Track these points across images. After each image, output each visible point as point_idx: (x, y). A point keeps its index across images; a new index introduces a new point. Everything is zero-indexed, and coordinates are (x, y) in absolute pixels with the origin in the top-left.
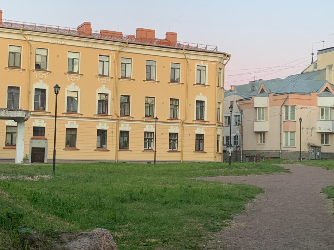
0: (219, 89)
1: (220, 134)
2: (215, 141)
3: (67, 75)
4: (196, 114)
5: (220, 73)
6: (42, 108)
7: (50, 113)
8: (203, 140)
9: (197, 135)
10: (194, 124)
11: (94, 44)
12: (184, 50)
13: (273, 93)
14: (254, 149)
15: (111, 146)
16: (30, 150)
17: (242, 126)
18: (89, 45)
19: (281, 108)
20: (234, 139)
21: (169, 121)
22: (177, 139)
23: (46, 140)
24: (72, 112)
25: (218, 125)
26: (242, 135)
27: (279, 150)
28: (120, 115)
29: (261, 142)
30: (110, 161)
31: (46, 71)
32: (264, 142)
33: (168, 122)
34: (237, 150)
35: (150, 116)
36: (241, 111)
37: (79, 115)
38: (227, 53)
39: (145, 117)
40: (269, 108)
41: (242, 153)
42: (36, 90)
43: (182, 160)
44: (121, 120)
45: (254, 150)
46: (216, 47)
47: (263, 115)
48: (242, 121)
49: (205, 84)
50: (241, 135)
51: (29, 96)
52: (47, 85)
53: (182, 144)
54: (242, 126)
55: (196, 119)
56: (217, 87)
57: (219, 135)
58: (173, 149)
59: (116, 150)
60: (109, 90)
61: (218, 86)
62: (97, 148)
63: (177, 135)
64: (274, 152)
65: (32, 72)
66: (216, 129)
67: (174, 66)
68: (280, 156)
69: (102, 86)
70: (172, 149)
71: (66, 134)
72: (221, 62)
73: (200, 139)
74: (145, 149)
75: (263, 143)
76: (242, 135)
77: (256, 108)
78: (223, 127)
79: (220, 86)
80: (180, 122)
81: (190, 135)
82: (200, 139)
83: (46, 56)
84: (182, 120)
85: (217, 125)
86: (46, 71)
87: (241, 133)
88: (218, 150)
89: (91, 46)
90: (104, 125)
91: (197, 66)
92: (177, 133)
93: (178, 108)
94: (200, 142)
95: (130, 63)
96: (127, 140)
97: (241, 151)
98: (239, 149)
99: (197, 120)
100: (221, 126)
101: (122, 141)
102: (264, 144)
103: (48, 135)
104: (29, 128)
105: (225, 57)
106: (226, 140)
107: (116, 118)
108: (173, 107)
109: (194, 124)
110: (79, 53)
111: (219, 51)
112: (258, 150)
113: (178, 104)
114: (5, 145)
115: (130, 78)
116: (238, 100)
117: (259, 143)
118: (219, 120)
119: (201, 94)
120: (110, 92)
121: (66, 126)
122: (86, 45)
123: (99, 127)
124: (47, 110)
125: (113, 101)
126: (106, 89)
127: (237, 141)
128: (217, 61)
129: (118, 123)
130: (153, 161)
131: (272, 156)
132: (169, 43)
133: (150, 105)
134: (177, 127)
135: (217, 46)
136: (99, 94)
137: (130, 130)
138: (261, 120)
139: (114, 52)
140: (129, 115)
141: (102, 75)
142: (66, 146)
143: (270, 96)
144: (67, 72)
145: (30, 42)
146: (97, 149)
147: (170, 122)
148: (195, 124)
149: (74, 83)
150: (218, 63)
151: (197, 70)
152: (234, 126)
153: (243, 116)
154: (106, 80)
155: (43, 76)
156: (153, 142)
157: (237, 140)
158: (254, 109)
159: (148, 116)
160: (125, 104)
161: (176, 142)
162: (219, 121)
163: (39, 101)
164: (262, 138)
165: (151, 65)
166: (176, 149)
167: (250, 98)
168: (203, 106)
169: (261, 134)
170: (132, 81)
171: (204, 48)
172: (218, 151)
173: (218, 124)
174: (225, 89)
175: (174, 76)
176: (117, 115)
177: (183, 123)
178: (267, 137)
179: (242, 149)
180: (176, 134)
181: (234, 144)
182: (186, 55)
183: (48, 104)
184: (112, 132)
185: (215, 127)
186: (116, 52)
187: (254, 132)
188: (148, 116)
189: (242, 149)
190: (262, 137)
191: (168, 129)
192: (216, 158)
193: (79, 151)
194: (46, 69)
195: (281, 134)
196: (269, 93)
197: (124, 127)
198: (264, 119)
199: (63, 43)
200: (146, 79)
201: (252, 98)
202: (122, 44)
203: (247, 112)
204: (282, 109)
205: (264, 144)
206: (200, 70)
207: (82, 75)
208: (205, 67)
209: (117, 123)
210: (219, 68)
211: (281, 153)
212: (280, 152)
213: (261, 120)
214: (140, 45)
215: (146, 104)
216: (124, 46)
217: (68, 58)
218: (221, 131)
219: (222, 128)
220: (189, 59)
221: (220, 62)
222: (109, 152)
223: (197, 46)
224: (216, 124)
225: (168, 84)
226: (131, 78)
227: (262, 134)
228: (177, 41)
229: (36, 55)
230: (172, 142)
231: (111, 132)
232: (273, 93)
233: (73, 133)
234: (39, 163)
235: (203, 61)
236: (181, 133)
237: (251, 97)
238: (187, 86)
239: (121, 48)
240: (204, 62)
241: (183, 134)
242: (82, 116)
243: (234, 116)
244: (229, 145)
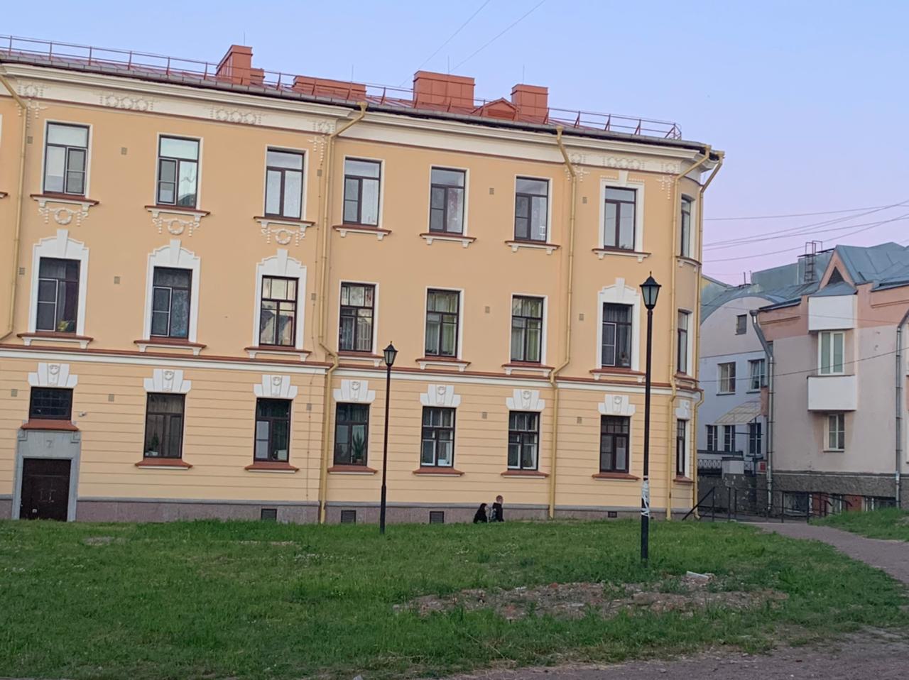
0: (681, 264)
1: (689, 418)
2: (668, 441)
3: (155, 212)
4: (39, 304)
5: (686, 215)
6: (65, 324)
7: (91, 340)
8: (627, 436)
9: (606, 419)
10: (508, 376)
11: (112, 93)
12: (559, 133)
13: (871, 284)
14: (810, 467)
15: (306, 456)
16: (17, 467)
17: (769, 393)
18: (234, 116)
19: (898, 331)
20: (749, 436)
21: (508, 371)
22: (534, 433)
23: (72, 434)
24: (170, 337)
25: (677, 386)
26: (770, 423)
27: (893, 471)
28: (337, 351)
29: (832, 444)
30: (628, 515)
31: (80, 198)
32: (842, 446)
33: (503, 376)
34: (757, 470)
35: (446, 353)
36: (768, 345)
37: (194, 348)
38: (708, 144)
39: (424, 356)
40: (857, 333)
41: (770, 480)
42: (45, 262)
43: (554, 505)
44: (340, 366)
45: (808, 469)
46: (673, 126)
47: (838, 356)
48: (771, 375)
49: (633, 250)
50: (768, 423)
51: (16, 283)
52: (82, 246)
53: (554, 449)
54: (769, 393)
55: (603, 366)
56: (674, 259)
57: (682, 422)
58: (522, 466)
59: (321, 469)
60: (300, 265)
61: (679, 254)
62: (255, 460)
63: (536, 418)
64: (875, 479)
65: (31, 201)
66: (672, 401)
67: (444, 179)
68: (895, 494)
69: (55, 234)
70: (518, 467)
71: (148, 413)
72: (687, 176)
73: (616, 432)
74: (423, 464)
75: (839, 448)
76: (770, 420)
77: (814, 334)
78: (699, 393)
79: (686, 255)
80: (546, 375)
81: (579, 419)
82: (618, 431)
83: (83, 151)
84: (553, 369)
85: (674, 387)
86: (82, 199)
87: (766, 416)
88: (681, 470)
89: (239, 117)
90: (280, 384)
91: (607, 187)
92: (538, 414)
93: (541, 329)
94: (618, 443)
95: (300, 168)
96: (362, 436)
97: (769, 474)
98: (763, 467)
99: (606, 368)
100: (690, 389)
101: (344, 439)
102: (843, 452)
103: (83, 415)
104: (14, 393)
105: (703, 158)
106: (726, 436)
107: (322, 359)
108: (524, 326)
109: (508, 376)
110: (198, 141)
111: (683, 139)
112: (824, 470)
113: (539, 316)
114: (599, 470)
115: (374, 228)
116: (757, 308)
117: (827, 447)
118: (682, 369)
119: (620, 281)
120: (87, 256)
121: (30, 380)
122: (222, 116)
123: (606, 409)
124: (80, 332)
125: (312, 302)
126: (627, 290)
127: (759, 441)
128: (676, 173)
129: (329, 377)
130: (378, 507)
131: (870, 494)
132: (511, 113)
133: (445, 316)
134: (535, 393)
135: (674, 125)
136: (516, 300)
137: (634, 414)
138: (832, 373)
139: (318, 139)
140: (371, 351)
141: (280, 216)
142: (147, 454)
143: (859, 293)
144: (155, 205)
145: (28, 103)
146: (334, 467)
147: (512, 376)
148: (600, 381)
149: (178, 242)
150: (679, 179)
151: (607, 201)
152: (748, 393)
153: (773, 360)
154: (291, 232)
155: (68, 215)
156: (451, 442)
157: (759, 437)
158: (808, 338)
159: (436, 353)
160: (357, 313)
161: (533, 443)
162: (685, 373)
163: (168, 311)
164: (837, 431)
165: (622, 199)
166: (535, 468)
167: (797, 303)
168: (629, 321)
169: (831, 417)
170: (380, 237)
171: (603, 127)
172: (680, 473)
173: (678, 383)
174: (705, 271)
175: (442, 212)
176: (328, 351)
177: (556, 378)
178: (854, 429)
179: (769, 467)
180: (533, 416)
181: (749, 451)
182: (569, 152)
183: (302, 328)
184: (309, 407)
185: (669, 392)
186: (326, 137)
187: (809, 411)
188: (438, 354)
189: (772, 467)
190: (835, 430)
191: (505, 397)
192: (670, 497)
193: (190, 472)
194: (83, 193)
195: (898, 419)
196: (856, 284)
197: (354, 388)
198: (841, 371)
199: (142, 106)
200: (431, 230)
201: (802, 302)
202: (344, 112)
203: (789, 350)
204: (903, 334)
205: (843, 452)
206: (620, 201)
207: (208, 214)
208: (635, 190)
209: (326, 376)
210: (684, 198)
211: (900, 485)
212: (898, 478)
213: (832, 373)
214: (138, 81)
215: (428, 312)
216: (351, 120)
217: (159, 156)
218: (691, 406)
219: (696, 396)
220: (579, 164)
221: (685, 177)
222: (297, 475)
223: (608, 124)
224: (673, 384)
225: (505, 247)
226: (462, 233)
227: (837, 418)
228: (475, 97)
229: (197, 161)
230: (519, 443)
231: (305, 406)
232: (871, 282)
233: (174, 409)
234: (792, 521)
235: (627, 172)
236: (548, 412)
237: (800, 300)
238: (571, 255)
239: (341, 125)
240: (629, 174)
241: (555, 417)
242: (204, 353)
243: (750, 363)
244: (730, 452)
